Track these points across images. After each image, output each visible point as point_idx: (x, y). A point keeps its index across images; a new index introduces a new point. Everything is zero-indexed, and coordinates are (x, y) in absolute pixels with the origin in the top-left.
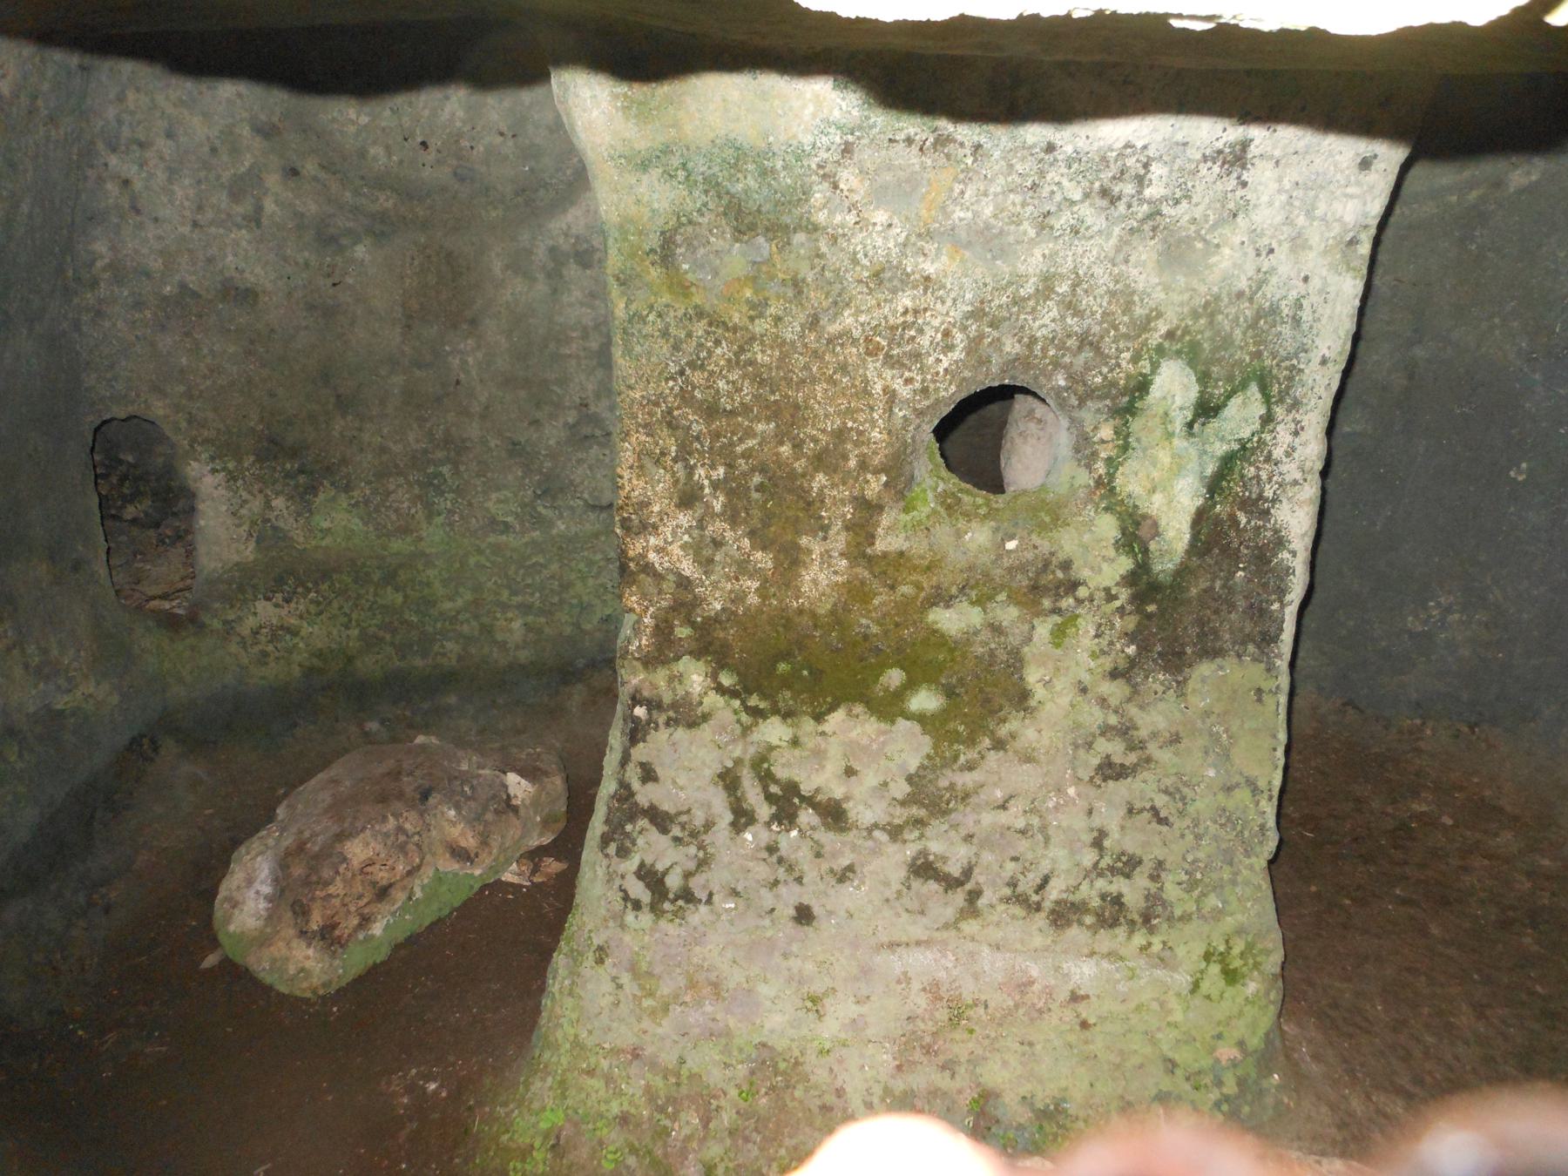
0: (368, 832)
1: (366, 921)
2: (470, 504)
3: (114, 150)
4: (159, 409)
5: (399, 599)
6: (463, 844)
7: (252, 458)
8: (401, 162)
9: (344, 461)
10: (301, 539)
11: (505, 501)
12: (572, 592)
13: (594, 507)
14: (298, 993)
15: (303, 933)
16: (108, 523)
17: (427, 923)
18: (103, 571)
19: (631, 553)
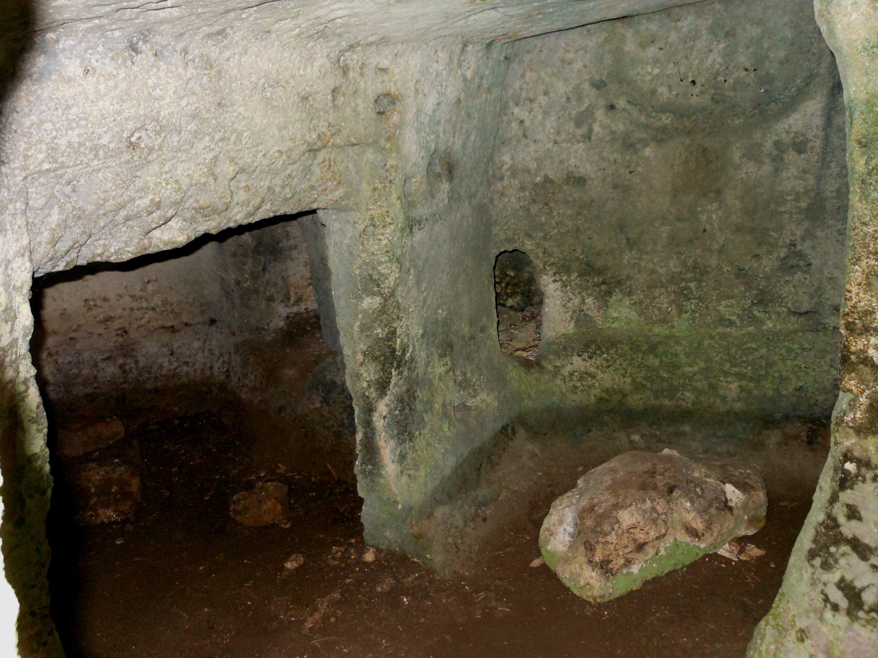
0: (633, 507)
1: (628, 563)
2: (707, 307)
3: (517, 105)
4: (528, 246)
5: (657, 362)
6: (694, 525)
7: (576, 275)
8: (677, 95)
9: (629, 278)
10: (600, 323)
11: (731, 306)
12: (775, 368)
13: (795, 313)
14: (585, 597)
15: (590, 562)
16: (500, 308)
17: (666, 571)
18: (495, 333)
19: (853, 349)
